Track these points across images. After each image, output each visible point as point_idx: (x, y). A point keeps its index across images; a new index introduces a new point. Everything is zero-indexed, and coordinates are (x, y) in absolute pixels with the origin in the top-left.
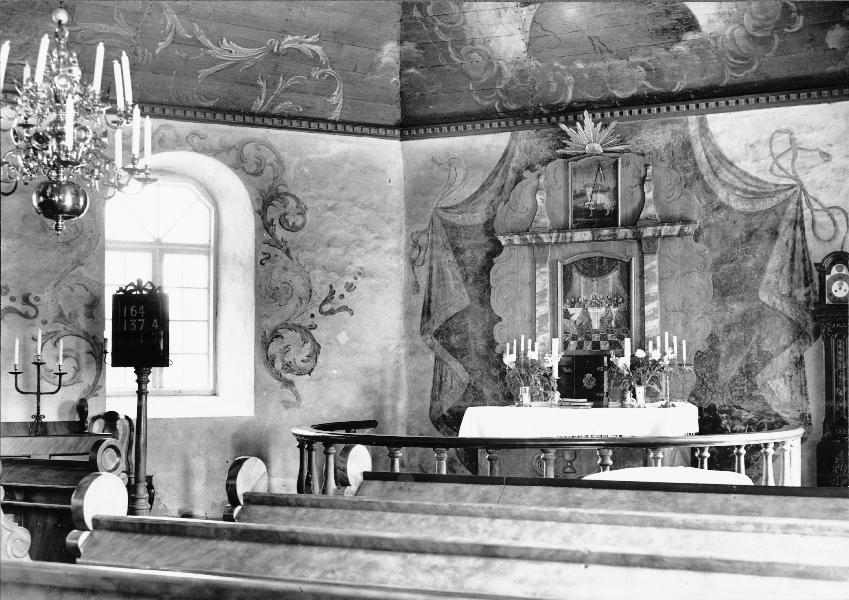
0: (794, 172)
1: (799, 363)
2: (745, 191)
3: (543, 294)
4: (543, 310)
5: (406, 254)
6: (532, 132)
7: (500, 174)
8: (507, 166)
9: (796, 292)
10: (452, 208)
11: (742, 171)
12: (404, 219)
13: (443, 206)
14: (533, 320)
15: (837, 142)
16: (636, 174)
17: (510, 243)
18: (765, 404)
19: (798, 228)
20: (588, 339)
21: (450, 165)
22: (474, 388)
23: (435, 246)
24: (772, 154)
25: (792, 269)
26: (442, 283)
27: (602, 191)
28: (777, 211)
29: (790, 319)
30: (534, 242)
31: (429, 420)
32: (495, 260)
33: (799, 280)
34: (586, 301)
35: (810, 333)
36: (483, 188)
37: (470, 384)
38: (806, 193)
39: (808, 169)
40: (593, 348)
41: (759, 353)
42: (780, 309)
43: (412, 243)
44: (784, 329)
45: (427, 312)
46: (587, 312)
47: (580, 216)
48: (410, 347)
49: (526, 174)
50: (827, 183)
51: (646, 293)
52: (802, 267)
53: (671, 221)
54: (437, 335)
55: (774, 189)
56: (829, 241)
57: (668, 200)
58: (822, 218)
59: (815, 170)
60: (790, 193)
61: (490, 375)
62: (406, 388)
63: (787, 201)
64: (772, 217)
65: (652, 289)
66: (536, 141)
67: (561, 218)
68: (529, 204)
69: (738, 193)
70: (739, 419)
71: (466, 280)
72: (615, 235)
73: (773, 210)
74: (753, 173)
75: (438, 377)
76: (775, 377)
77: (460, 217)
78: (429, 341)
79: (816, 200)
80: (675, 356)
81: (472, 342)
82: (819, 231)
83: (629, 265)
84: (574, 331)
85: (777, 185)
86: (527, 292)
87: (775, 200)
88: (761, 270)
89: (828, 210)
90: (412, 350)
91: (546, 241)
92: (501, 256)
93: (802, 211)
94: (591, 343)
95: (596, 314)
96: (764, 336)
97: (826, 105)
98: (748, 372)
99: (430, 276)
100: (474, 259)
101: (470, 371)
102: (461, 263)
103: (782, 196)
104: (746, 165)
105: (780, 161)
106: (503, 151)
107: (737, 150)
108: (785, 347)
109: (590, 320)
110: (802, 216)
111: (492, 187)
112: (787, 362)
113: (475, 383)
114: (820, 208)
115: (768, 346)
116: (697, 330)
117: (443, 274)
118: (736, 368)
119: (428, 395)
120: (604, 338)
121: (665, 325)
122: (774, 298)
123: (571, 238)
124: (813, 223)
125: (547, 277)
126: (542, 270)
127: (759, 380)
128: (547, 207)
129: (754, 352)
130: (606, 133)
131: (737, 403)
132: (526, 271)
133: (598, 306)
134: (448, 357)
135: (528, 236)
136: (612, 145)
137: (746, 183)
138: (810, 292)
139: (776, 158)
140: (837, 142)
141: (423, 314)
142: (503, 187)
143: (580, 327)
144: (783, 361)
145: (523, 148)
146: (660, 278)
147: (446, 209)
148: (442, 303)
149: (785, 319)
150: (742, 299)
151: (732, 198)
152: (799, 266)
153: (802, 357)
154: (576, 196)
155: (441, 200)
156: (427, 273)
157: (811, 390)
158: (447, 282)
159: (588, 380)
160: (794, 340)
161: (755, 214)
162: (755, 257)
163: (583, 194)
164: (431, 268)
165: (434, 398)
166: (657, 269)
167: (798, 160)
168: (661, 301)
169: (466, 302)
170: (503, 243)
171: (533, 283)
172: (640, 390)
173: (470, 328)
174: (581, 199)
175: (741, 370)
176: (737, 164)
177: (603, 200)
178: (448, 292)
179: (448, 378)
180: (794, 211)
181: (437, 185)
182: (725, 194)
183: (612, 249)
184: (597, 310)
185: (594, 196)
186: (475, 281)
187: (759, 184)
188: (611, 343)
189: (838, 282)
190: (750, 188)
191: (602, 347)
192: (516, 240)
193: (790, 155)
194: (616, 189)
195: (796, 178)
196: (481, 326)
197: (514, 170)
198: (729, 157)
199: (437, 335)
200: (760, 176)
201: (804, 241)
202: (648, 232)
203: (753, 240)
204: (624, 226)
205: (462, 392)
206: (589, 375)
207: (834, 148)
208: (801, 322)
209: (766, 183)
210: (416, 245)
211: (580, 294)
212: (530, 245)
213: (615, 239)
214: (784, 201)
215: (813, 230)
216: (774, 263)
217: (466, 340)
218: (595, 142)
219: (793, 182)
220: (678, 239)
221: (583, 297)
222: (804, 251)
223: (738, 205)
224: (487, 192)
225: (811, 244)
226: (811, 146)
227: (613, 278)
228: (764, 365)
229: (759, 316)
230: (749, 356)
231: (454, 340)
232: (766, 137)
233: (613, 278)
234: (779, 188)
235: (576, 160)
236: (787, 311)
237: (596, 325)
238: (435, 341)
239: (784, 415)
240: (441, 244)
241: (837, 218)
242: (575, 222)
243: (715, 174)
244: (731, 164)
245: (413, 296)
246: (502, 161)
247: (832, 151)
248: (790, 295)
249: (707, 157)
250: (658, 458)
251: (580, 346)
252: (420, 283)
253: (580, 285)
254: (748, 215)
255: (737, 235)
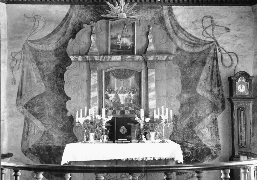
0: (213, 35)
1: (215, 121)
2: (190, 43)
3: (94, 86)
4: (94, 94)
5: (8, 64)
6: (82, 6)
7: (64, 26)
8: (68, 22)
9: (214, 90)
10: (36, 41)
11: (188, 34)
12: (7, 45)
13: (32, 39)
14: (89, 99)
15: (233, 23)
16: (144, 29)
17: (76, 60)
18: (199, 140)
19: (215, 61)
20: (119, 109)
21: (35, 18)
22: (47, 134)
23: (25, 60)
24: (203, 27)
25: (212, 79)
26: (29, 79)
27: (126, 37)
28: (205, 53)
29: (211, 102)
30: (90, 60)
31: (21, 151)
32: (67, 68)
33: (215, 84)
34: (117, 90)
35: (220, 108)
36: (54, 32)
37: (45, 132)
38: (218, 45)
39: (220, 35)
40: (121, 114)
41: (196, 117)
42: (206, 97)
43: (11, 58)
44: (208, 106)
45: (20, 94)
46: (118, 96)
47: (114, 49)
48: (10, 113)
49: (85, 25)
50: (228, 41)
51: (149, 87)
52: (216, 78)
53: (162, 53)
54: (26, 106)
55: (203, 43)
56: (229, 67)
57: (160, 44)
58: (226, 57)
59: (222, 35)
60: (211, 45)
61: (56, 127)
62: (7, 134)
63: (210, 48)
64: (202, 55)
65: (152, 85)
66: (84, 10)
67: (104, 49)
68: (87, 40)
69: (186, 43)
70: (187, 147)
71: (43, 78)
72: (133, 58)
73: (203, 51)
74: (194, 35)
75: (26, 128)
76: (203, 128)
77: (41, 46)
78: (21, 110)
79: (223, 49)
80: (167, 117)
81: (47, 110)
82: (224, 62)
83: (140, 74)
84: (111, 105)
85: (205, 41)
86: (85, 85)
87: (204, 47)
88: (197, 79)
89: (229, 53)
90: (11, 114)
91: (96, 59)
92: (70, 66)
93: (217, 53)
94: (120, 111)
95: (123, 97)
96: (199, 109)
97: (228, 6)
98: (191, 126)
99: (23, 75)
100: (48, 69)
101: (45, 125)
102: (41, 70)
103: (207, 46)
104: (190, 31)
105: (207, 30)
106: (65, 14)
107: (186, 24)
108: (209, 114)
109: (119, 100)
110: (217, 56)
111: (59, 32)
112: (209, 121)
113: (48, 131)
114: (225, 52)
115: (200, 113)
116: (174, 106)
117: (30, 74)
118: (185, 124)
119: (20, 138)
120: (127, 109)
121: (158, 104)
122: (204, 92)
123: (110, 59)
124: (222, 59)
125: (96, 78)
126: (95, 74)
127: (196, 129)
128: (96, 43)
129: (194, 116)
130: (131, 8)
131: (186, 140)
132: (85, 75)
133: (124, 93)
134: (32, 118)
135: (87, 57)
136: (132, 15)
137: (190, 39)
138: (220, 90)
139: (205, 29)
140: (233, 23)
141: (18, 95)
142: (66, 32)
143: (114, 103)
144: (208, 120)
145: (77, 13)
146: (156, 80)
147: (32, 42)
148: (29, 90)
149: (209, 102)
150: (188, 92)
151: (184, 46)
152: (215, 78)
153: (216, 119)
154: (112, 39)
155: (29, 36)
156: (21, 74)
157: (220, 134)
158: (32, 79)
159: (123, 130)
160: (213, 111)
161: (195, 53)
162: (194, 73)
163: (116, 38)
164: (23, 72)
165: (24, 139)
166: (154, 76)
167: (215, 30)
168: (156, 91)
169: (43, 89)
170: (72, 60)
171: (89, 81)
172: (92, 136)
173: (46, 103)
174: (115, 40)
175: (188, 124)
176: (186, 30)
177: (127, 41)
178: (33, 84)
179: (33, 130)
180: (213, 53)
181: (27, 29)
182: (180, 43)
183: (132, 66)
184: (123, 95)
185: (122, 39)
186: (49, 79)
187: (197, 40)
188: (130, 111)
189: (240, 85)
190: (192, 42)
191: (126, 113)
192: (80, 58)
193: (211, 27)
194: (134, 36)
195: (214, 38)
196: (52, 102)
197: (72, 24)
198: (182, 26)
199: (26, 106)
200: (197, 36)
201: (217, 66)
202: (151, 58)
203: (194, 65)
204: (138, 54)
205: (40, 135)
206: (123, 127)
207: (232, 26)
208: (216, 103)
209: (200, 40)
210: (14, 59)
211: (114, 86)
212: (88, 62)
213: (133, 61)
214: (208, 48)
215: (222, 62)
216: (203, 76)
217: (43, 109)
218: (123, 12)
219: (212, 40)
220: (165, 62)
221: (116, 89)
222: (217, 71)
223: (187, 49)
224: (56, 34)
225: (221, 68)
226: (221, 25)
227: (132, 80)
228: (199, 122)
229: (197, 100)
230: (191, 118)
231: (36, 109)
232: (200, 18)
233: (132, 80)
234: (206, 42)
235: (113, 21)
236: (210, 98)
237: (123, 102)
238: (25, 110)
239: (207, 145)
240: (29, 59)
241: (233, 57)
242: (111, 51)
243: (176, 34)
244: (183, 30)
245: (12, 86)
246: (65, 19)
247: (230, 27)
248: (211, 91)
249: (172, 26)
250: (247, 173)
251: (114, 113)
252: (16, 79)
253: (114, 82)
254: (192, 54)
255: (186, 63)
